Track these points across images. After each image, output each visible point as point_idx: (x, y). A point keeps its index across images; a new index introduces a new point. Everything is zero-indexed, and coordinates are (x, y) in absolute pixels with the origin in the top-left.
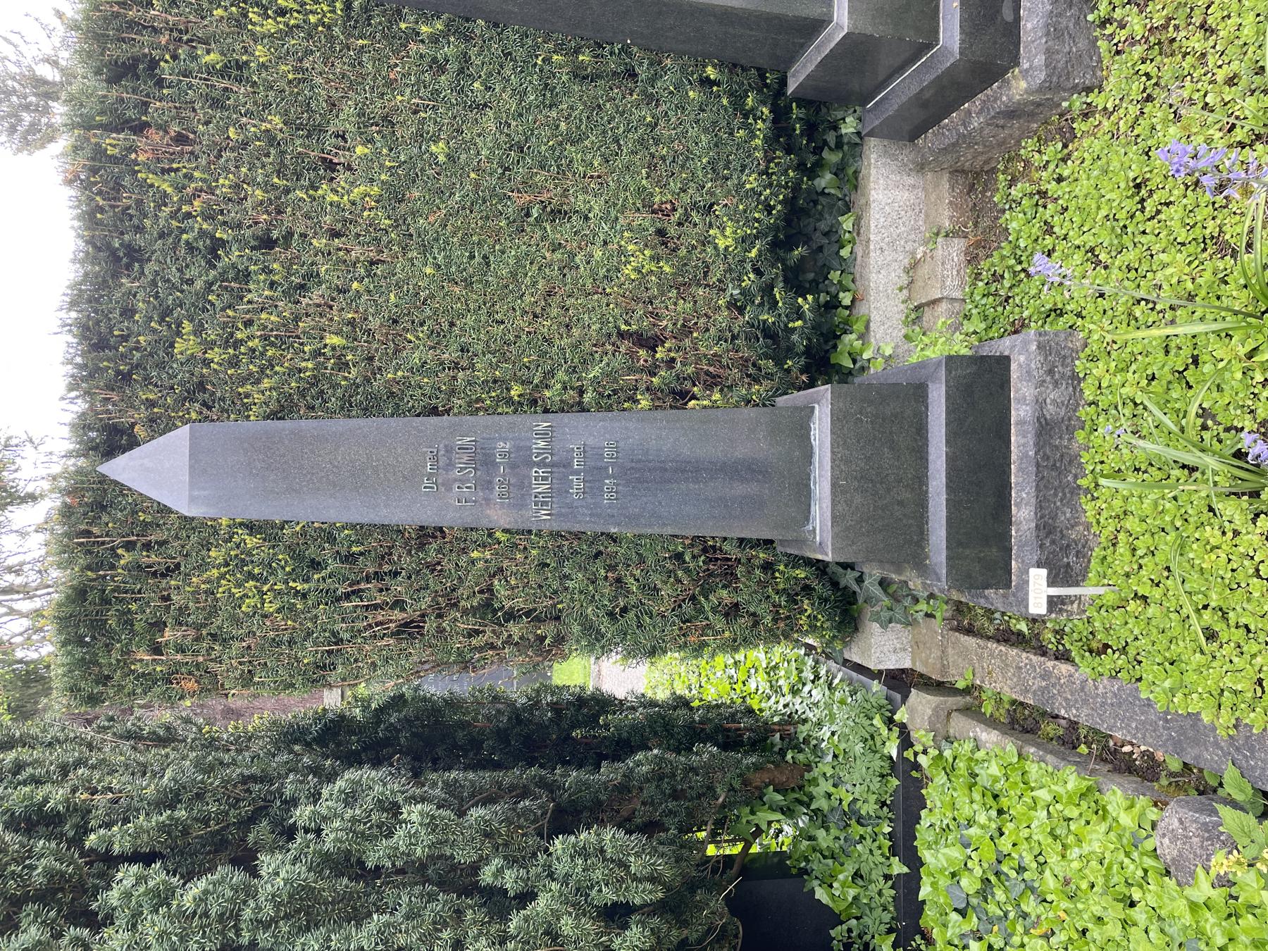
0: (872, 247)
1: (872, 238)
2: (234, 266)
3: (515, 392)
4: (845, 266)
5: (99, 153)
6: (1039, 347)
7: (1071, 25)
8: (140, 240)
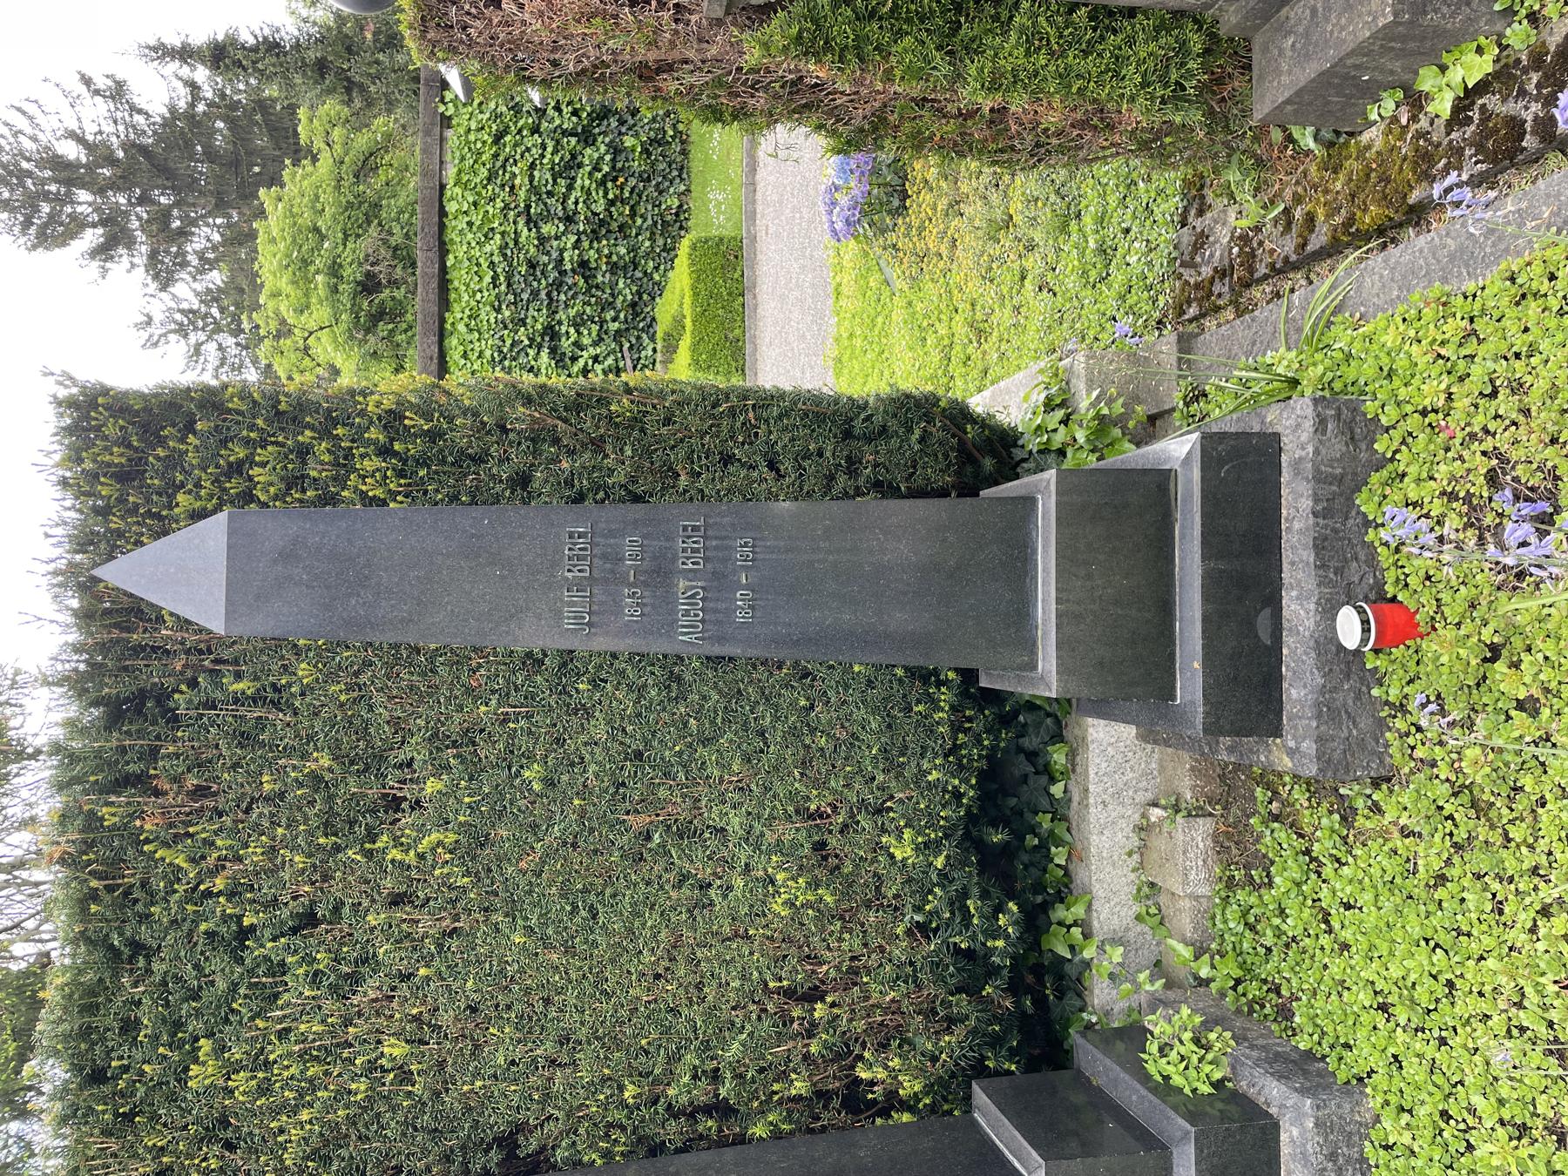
0: (1091, 801)
1: (1092, 788)
2: (267, 959)
3: (629, 1092)
4: (1059, 811)
5: (92, 821)
6: (1316, 1125)
7: (1350, 702)
8: (144, 934)
